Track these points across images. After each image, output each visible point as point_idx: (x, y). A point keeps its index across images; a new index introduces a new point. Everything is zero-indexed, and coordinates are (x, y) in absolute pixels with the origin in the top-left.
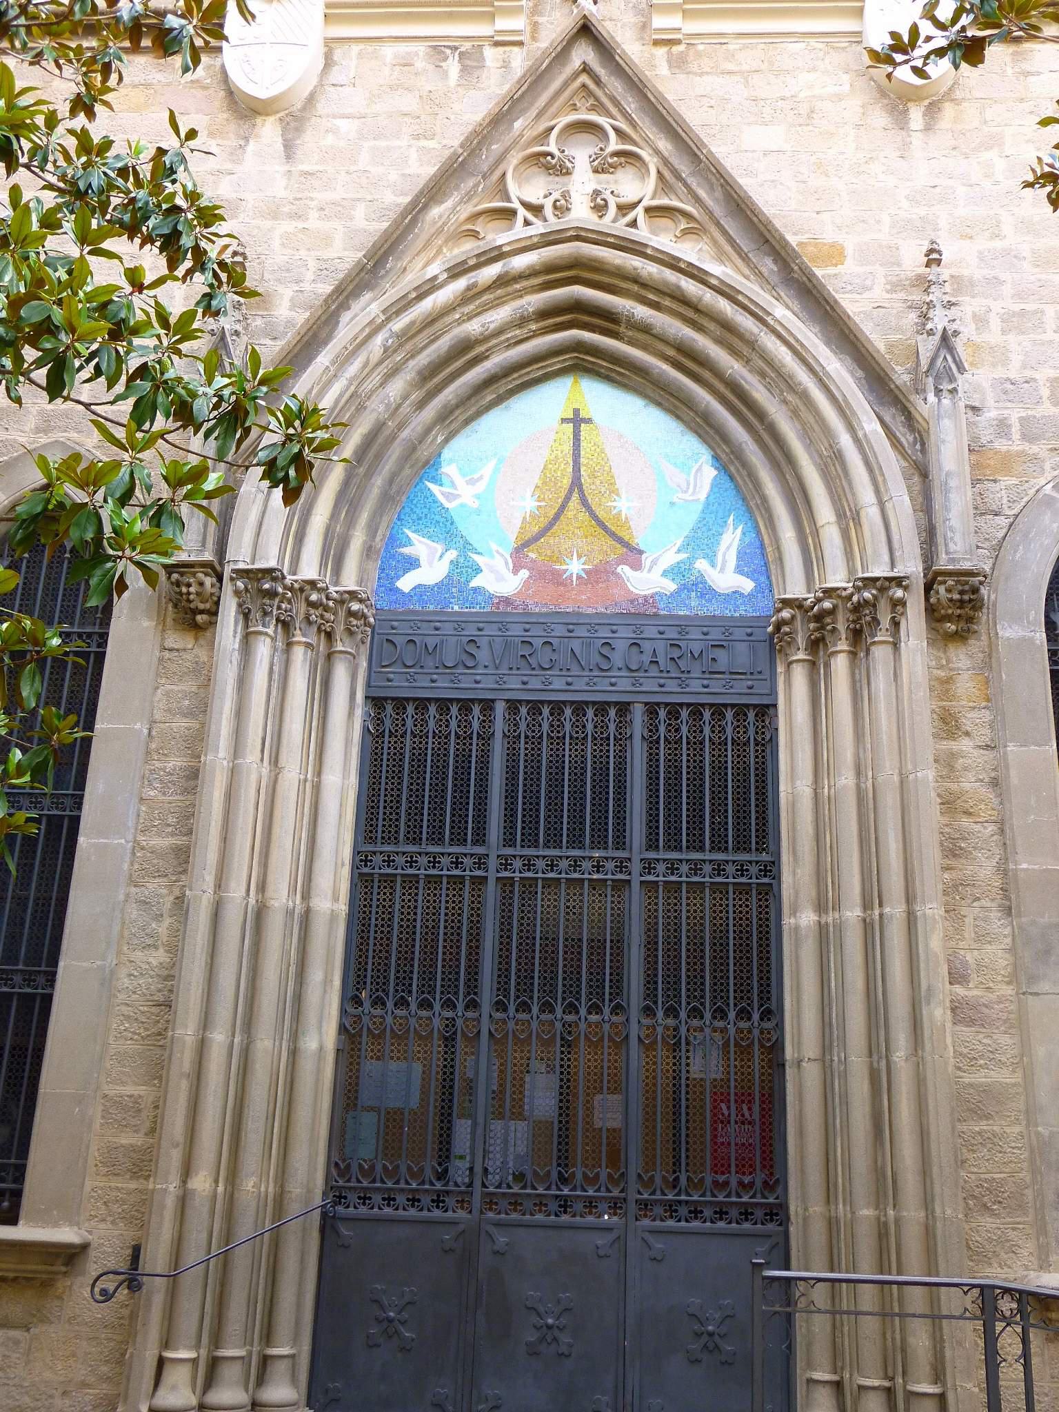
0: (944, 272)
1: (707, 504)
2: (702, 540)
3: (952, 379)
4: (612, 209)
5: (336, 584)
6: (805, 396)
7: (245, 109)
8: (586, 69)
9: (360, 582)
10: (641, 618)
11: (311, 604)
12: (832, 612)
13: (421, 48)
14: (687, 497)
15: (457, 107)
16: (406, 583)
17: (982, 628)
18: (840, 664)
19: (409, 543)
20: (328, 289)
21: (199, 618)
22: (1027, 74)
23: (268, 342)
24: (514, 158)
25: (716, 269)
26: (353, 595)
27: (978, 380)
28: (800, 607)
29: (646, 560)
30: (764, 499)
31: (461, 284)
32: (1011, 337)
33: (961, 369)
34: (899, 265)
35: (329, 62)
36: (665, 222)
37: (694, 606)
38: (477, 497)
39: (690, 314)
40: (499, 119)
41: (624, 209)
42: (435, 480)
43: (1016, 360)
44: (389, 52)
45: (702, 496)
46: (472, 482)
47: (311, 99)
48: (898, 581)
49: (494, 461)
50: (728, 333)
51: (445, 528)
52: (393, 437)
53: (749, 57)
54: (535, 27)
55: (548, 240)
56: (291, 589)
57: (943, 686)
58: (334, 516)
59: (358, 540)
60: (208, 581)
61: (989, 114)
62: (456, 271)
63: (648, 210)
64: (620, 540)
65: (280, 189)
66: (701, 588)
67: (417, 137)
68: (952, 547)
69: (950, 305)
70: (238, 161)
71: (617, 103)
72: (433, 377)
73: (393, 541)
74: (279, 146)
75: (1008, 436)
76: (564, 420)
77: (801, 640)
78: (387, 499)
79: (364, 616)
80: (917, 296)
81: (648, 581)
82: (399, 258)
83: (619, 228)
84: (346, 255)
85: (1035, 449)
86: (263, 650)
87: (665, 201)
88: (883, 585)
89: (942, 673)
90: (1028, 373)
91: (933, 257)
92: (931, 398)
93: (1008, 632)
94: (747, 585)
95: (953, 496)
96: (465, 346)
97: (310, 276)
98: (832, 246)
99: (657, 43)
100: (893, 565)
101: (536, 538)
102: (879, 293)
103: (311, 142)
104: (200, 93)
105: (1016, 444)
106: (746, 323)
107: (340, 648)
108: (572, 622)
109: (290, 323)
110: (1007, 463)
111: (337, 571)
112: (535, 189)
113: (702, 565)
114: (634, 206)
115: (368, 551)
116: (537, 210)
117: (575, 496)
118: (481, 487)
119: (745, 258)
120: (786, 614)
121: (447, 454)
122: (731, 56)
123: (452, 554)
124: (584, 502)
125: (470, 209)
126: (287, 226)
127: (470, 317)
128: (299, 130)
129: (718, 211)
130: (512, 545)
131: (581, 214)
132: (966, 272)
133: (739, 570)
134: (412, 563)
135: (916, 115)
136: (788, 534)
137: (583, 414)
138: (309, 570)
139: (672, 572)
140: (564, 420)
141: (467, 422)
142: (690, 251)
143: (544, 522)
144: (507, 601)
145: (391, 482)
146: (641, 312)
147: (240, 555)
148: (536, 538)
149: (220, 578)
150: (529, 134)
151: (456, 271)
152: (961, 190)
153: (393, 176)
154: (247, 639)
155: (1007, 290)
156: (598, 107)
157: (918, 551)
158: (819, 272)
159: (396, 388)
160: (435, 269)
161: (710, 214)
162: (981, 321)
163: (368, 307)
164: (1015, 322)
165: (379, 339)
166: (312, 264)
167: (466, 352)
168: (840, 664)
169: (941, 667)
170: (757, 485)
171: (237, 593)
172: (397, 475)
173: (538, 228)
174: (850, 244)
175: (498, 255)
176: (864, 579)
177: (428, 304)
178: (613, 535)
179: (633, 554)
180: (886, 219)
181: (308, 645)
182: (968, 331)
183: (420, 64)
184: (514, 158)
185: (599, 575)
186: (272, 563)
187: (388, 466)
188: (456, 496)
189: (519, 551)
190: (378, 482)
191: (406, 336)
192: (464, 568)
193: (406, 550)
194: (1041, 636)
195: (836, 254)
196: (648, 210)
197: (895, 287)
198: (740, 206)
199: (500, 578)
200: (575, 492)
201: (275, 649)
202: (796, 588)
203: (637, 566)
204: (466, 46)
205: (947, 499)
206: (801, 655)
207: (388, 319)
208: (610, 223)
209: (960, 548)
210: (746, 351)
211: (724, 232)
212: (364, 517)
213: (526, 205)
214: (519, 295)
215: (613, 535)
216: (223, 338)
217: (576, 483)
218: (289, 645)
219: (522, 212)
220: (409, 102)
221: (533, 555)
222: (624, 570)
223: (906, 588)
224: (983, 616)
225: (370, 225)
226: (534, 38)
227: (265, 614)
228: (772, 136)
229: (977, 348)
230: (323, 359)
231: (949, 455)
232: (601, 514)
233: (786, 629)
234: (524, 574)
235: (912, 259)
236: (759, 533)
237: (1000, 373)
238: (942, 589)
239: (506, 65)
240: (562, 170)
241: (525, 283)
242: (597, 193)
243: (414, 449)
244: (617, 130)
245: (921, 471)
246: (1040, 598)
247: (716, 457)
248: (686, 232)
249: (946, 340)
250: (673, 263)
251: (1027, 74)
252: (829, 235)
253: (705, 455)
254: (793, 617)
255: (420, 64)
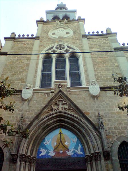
0: (101, 115)
1: (76, 143)
2: (76, 148)
3: (103, 127)
4: (64, 109)
5: (32, 155)
6: (86, 129)
7: (23, 100)
8: (60, 95)
9: (35, 155)
10: (70, 157)
11: (29, 159)
12: (92, 157)
13: (43, 93)
14: (74, 142)
15: (47, 99)
16: (40, 155)
17: (110, 158)
18: (94, 163)
19: (41, 150)
20: (32, 119)
21: (15, 161)
22: (107, 94)
23: (25, 126)
24: (53, 104)
25: (76, 116)
26: (34, 157)
27: (106, 127)
28: (89, 156)
29: (70, 150)
30: (83, 142)
31: (47, 118)
32: (109, 122)
33: (104, 126)
34: (88, 39)
35: (33, 95)
36: (70, 110)
37: (76, 156)
38: (49, 143)
39: (73, 120)
40: (51, 100)
41: (65, 109)
42: (44, 142)
43: (110, 125)
44: (40, 94)
45: (76, 142)
46: (48, 141)
47: (31, 99)
48: (100, 152)
49: (51, 139)
50: (78, 123)
51: (45, 148)
52: (39, 136)
53: (77, 93)
54: (55, 91)
55: (57, 113)
56: (26, 157)
57: (107, 166)
58: (32, 147)
59: (35, 150)
60: (16, 156)
61: (103, 98)
62: (47, 117)
63: (68, 109)
64: (66, 148)
65: (27, 108)
66: (76, 154)
67: (42, 102)
68: (106, 148)
69: (101, 119)
70: (23, 106)
71: (64, 98)
72: (44, 129)
73: (39, 149)
74: (27, 104)
75: (110, 134)
76: (59, 133)
77: (89, 160)
78: (39, 144)
79: (35, 160)
80: (98, 118)
81: (70, 153)
82: (40, 115)
83: (65, 111)
84: (34, 115)
85: (113, 135)
86: (23, 165)
87: (70, 108)
88: (98, 153)
89: (106, 164)
90: (111, 126)
91: (99, 114)
92: (101, 129)
93: (114, 158)
94: (82, 153)
95: (105, 141)
96: (48, 125)
97: (30, 118)
98: (88, 112)
99: (68, 92)
100: (99, 150)
101: (56, 148)
102: (94, 117)
103: (31, 103)
104: (19, 99)
105: (111, 135)
106: (79, 121)
107: (32, 164)
108: (61, 159)
109: (28, 123)
110: (111, 137)
111: (32, 154)
112: (55, 107)
113: (76, 151)
114: (66, 109)
115: (36, 151)
116: (56, 109)
117: (61, 143)
118: (50, 142)
119: (79, 114)
120: (87, 157)
121: (45, 138)
122: (75, 93)
123: (46, 151)
124: (62, 143)
125: (48, 110)
126: (28, 112)
127: (49, 122)
128: (30, 102)
129: (75, 109)
130: (53, 149)
131: (60, 110)
132: (103, 115)
133: (81, 151)
134: (41, 152)
135: (96, 99)
136: (86, 146)
137: (61, 132)
138: (29, 154)
139: (73, 152)
140: (59, 133)
141: (48, 134)
142: (72, 113)
143: (57, 146)
144: (53, 157)
145: (39, 142)
146: (68, 120)
147: (20, 153)
148: (56, 148)
149: (17, 156)
150: (55, 102)
151: (47, 117)
152: (101, 106)
153: (40, 106)
154: (21, 164)
155: (108, 117)
156: (62, 98)
157: (101, 148)
158: (87, 115)
159: (40, 130)
160: (44, 117)
161: (74, 109)
162: (105, 120)
163: (37, 121)
164: (109, 120)
165: (38, 125)
166: (30, 117)
167: (48, 126)
168: (94, 163)
169: (106, 163)
170: (82, 141)
171: (20, 158)
172: (39, 141)
173: (56, 112)
174: (90, 112)
175: (51, 115)
176: (96, 152)
177: (43, 120)
178: (65, 147)
179: (68, 150)
180: (94, 110)
181: (28, 164)
182: (104, 121)
183: (43, 95)
184: (53, 104)
185: (64, 153)
186: (24, 154)
187: (39, 140)
188: (47, 143)
189: (54, 150)
190: (37, 142)
191: (41, 124)
192: (48, 153)
193: (40, 151)
194: (118, 159)
195: (89, 113)
196: (68, 109)
197: (95, 117)
198: (78, 108)
199: (52, 154)
200: (61, 142)
201: (24, 165)
202: (88, 154)
203: (68, 151)
204: (48, 93)
205: (104, 142)
206: (89, 162)
207: (39, 123)
208: (63, 111)
209: (107, 148)
210: (80, 125)
211: (76, 112)
212: (36, 146)
213: (54, 109)
214: (54, 119)
215: (65, 147)
216: (20, 126)
217: (61, 141)
218: (26, 165)
219: (54, 110)
220: (42, 99)
221: (56, 150)
222: (67, 152)
223: (101, 153)
224: (110, 156)
225: (37, 112)
226: (55, 92)
227: (23, 160)
228: (81, 101)
229: (105, 123)
230: (31, 128)
231: (104, 136)
232: (64, 145)
233: (87, 159)
234: (55, 153)
235: (97, 114)
236: (83, 147)
237: (108, 126)
238: (105, 153)
239: (52, 94)
240: (58, 105)
241: (55, 118)
242: (62, 107)
243: (42, 138)
244: (64, 101)
245: (101, 138)
246: (120, 52)
247: (77, 137)
248: (72, 111)
249: (102, 123)
250: (71, 115)
251: (107, 94)
252: (88, 111)
253: (76, 137)
254: (88, 157)
255: (43, 95)
